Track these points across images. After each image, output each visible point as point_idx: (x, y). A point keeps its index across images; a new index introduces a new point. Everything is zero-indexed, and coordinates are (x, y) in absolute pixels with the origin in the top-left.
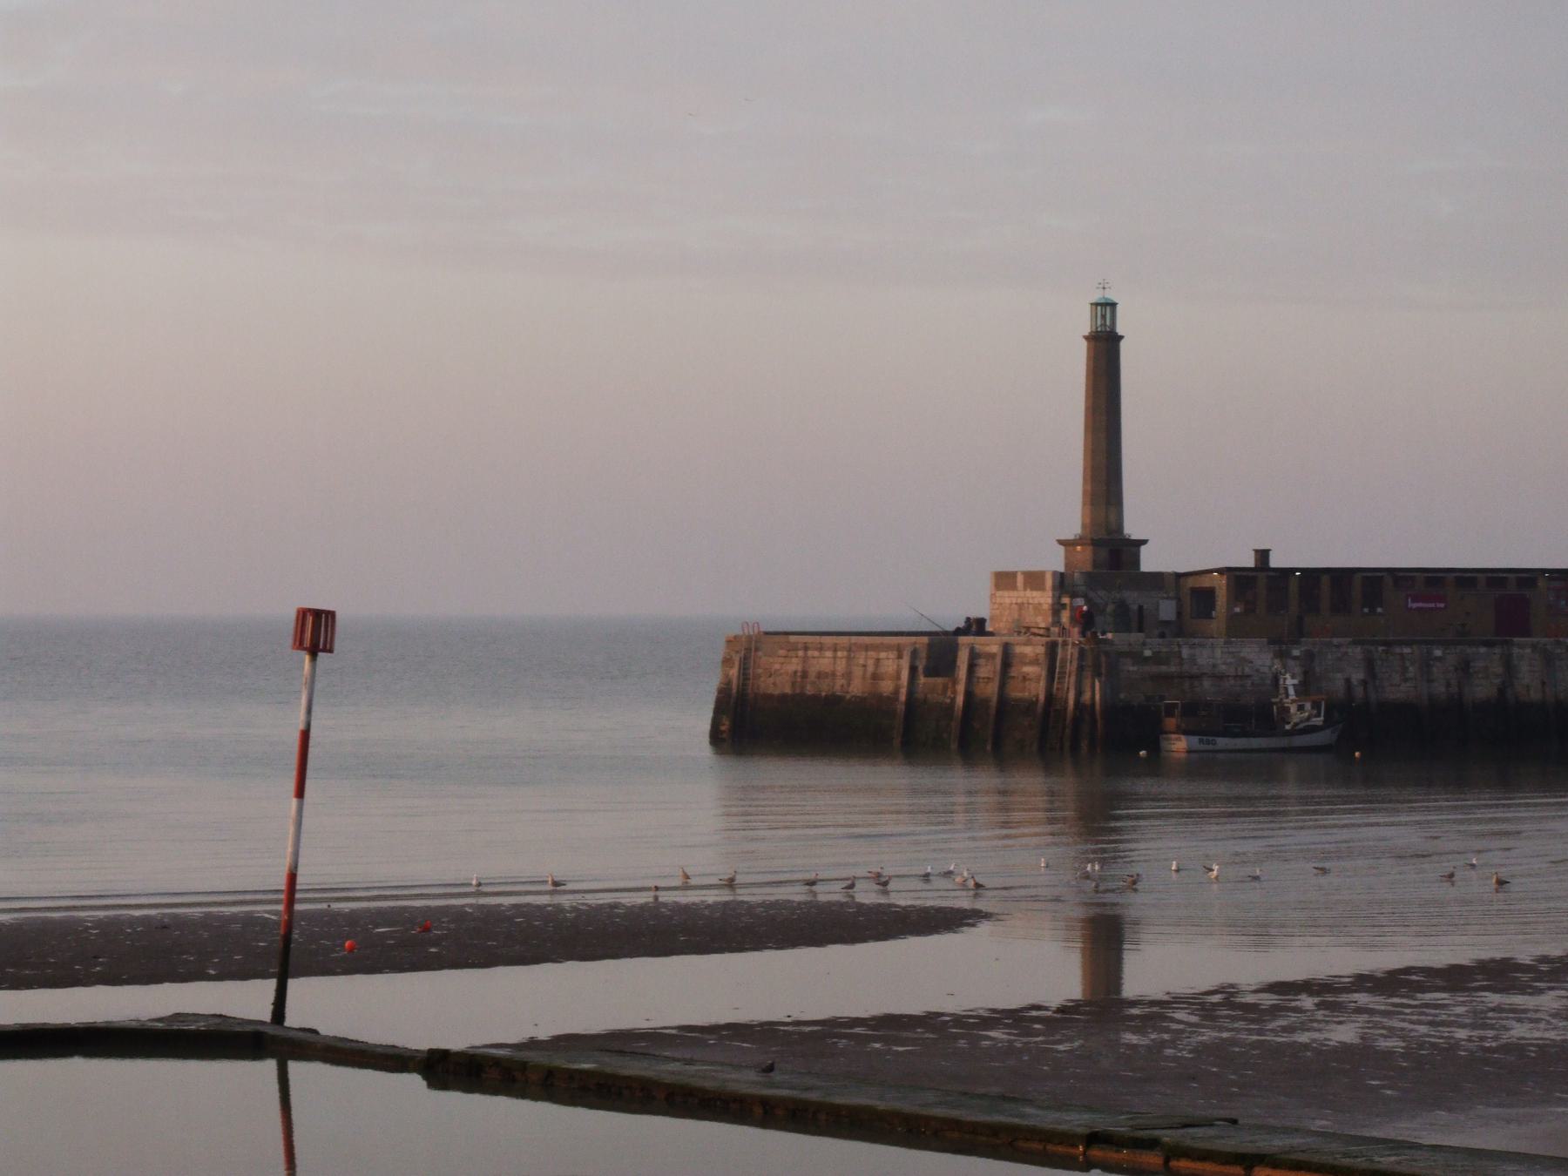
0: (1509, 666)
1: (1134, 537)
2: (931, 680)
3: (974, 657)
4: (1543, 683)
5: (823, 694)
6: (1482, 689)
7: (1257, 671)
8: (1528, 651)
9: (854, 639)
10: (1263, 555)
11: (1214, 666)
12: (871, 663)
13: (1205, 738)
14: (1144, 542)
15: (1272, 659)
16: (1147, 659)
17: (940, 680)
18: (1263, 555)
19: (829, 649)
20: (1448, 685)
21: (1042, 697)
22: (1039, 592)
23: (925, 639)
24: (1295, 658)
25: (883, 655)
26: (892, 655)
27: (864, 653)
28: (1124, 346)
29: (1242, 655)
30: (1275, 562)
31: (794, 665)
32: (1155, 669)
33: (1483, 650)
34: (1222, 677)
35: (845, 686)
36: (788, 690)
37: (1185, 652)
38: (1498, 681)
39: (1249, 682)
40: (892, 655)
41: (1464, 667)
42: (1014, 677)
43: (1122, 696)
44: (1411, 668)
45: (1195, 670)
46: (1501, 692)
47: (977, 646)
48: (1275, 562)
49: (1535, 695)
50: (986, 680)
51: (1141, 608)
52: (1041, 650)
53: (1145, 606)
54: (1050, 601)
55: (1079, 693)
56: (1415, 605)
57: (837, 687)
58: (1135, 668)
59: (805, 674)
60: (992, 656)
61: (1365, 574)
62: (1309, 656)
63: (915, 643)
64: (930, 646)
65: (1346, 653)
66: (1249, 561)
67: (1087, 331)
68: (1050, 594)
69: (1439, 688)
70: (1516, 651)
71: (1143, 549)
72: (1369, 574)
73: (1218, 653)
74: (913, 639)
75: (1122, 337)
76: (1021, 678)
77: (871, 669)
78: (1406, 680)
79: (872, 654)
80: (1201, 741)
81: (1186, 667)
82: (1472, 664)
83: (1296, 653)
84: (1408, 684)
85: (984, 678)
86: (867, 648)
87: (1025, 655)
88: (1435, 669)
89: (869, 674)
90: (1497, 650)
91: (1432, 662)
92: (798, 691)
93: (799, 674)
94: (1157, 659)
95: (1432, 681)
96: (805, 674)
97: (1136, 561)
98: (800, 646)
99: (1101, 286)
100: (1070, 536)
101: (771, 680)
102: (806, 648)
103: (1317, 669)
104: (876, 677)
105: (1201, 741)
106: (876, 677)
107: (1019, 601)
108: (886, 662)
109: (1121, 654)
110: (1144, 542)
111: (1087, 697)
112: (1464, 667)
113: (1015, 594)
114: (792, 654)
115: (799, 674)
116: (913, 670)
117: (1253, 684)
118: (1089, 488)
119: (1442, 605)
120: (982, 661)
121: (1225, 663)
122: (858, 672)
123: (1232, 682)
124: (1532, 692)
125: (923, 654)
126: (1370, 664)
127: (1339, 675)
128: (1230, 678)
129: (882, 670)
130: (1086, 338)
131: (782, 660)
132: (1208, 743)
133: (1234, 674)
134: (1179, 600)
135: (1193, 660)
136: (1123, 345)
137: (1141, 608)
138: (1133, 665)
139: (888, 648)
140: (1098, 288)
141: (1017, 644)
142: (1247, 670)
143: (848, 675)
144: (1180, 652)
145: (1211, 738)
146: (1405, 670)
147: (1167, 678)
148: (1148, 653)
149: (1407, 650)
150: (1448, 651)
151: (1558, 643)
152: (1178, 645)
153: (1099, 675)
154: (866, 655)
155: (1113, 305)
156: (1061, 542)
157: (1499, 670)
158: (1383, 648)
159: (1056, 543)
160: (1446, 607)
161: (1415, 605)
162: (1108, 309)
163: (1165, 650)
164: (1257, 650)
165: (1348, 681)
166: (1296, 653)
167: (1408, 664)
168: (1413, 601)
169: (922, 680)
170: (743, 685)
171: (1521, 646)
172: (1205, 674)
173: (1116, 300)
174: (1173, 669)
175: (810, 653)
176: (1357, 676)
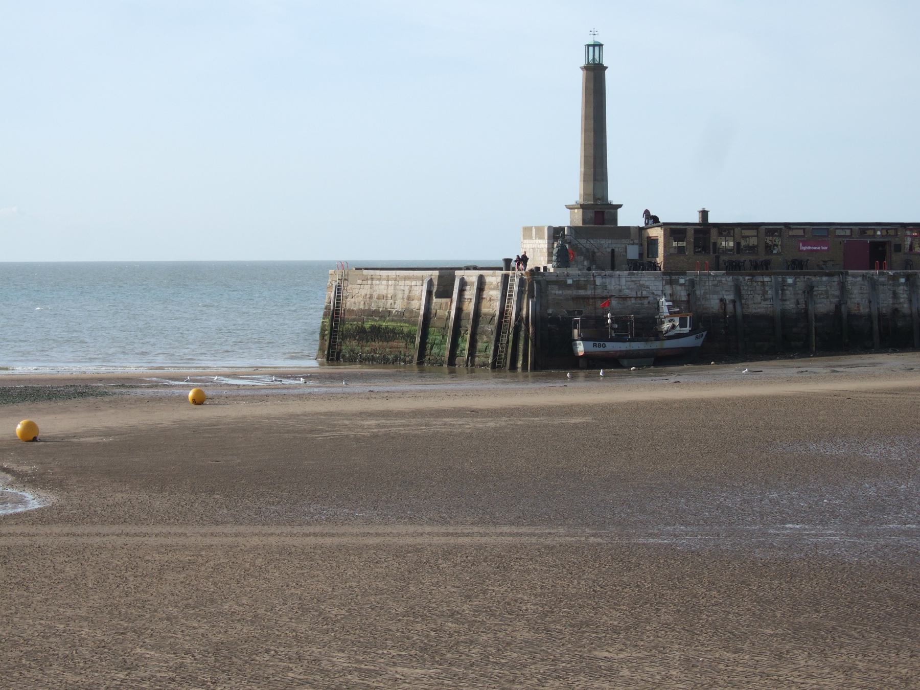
0: (842, 287)
1: (614, 203)
2: (439, 300)
3: (463, 283)
4: (870, 302)
5: (381, 309)
6: (824, 305)
7: (653, 293)
8: (860, 279)
9: (398, 272)
10: (704, 214)
11: (620, 291)
12: (407, 289)
13: (597, 343)
14: (620, 206)
15: (663, 286)
16: (570, 285)
17: (444, 300)
18: (704, 214)
19: (384, 279)
20: (798, 303)
21: (497, 313)
22: (542, 240)
23: (437, 273)
24: (682, 285)
25: (414, 283)
26: (419, 283)
27: (404, 282)
28: (608, 75)
29: (641, 282)
30: (711, 220)
31: (366, 290)
32: (575, 292)
33: (824, 279)
34: (625, 298)
35: (393, 304)
36: (362, 307)
37: (598, 281)
38: (835, 300)
39: (646, 302)
40: (419, 283)
41: (810, 290)
42: (485, 298)
43: (550, 311)
44: (769, 292)
45: (605, 294)
46: (838, 307)
47: (465, 277)
48: (711, 220)
49: (864, 310)
50: (469, 300)
51: (613, 251)
52: (499, 279)
53: (616, 250)
54: (546, 246)
55: (519, 309)
56: (805, 248)
57: (388, 305)
58: (560, 292)
59: (371, 297)
60: (472, 283)
61: (767, 227)
62: (692, 283)
63: (431, 275)
64: (440, 277)
65: (720, 281)
66: (696, 219)
67: (583, 63)
68: (547, 240)
69: (790, 305)
70: (850, 279)
71: (619, 210)
72: (771, 227)
73: (623, 281)
74: (430, 272)
75: (607, 68)
76: (488, 299)
77: (407, 293)
78: (765, 300)
79: (408, 282)
80: (594, 345)
81: (599, 292)
82: (815, 289)
83: (682, 281)
84: (766, 303)
85: (468, 299)
86: (405, 278)
87: (491, 284)
88: (787, 292)
89: (406, 296)
90: (836, 279)
91: (785, 288)
92: (367, 308)
93: (368, 296)
94: (577, 285)
95: (785, 300)
96: (371, 297)
97: (615, 219)
98: (369, 277)
99: (593, 32)
100: (572, 202)
101: (353, 300)
102: (372, 279)
103: (698, 292)
104: (409, 298)
105: (594, 345)
106: (409, 298)
107: (533, 246)
108: (415, 288)
109: (549, 283)
110: (620, 206)
111: (524, 312)
112: (810, 290)
113: (532, 241)
114: (365, 282)
115: (368, 296)
116: (429, 293)
117: (649, 302)
118: (583, 170)
119: (826, 248)
120: (468, 288)
121: (628, 289)
122: (400, 295)
123: (633, 301)
124: (861, 308)
125: (436, 282)
126: (738, 290)
127: (715, 296)
128: (633, 299)
129: (412, 294)
130: (582, 68)
131: (358, 287)
132: (600, 346)
133: (635, 296)
134: (641, 245)
135: (604, 287)
136: (607, 72)
137: (613, 251)
138: (559, 290)
139: (415, 278)
140: (590, 35)
141: (488, 275)
142: (645, 293)
143: (394, 297)
144: (595, 281)
145: (602, 343)
146: (765, 293)
147: (585, 299)
148: (570, 282)
149: (766, 279)
150: (798, 280)
151: (881, 274)
152: (593, 276)
153: (533, 297)
154: (405, 283)
155: (600, 46)
156: (647, 213)
157: (837, 293)
158: (749, 278)
159: (565, 207)
160: (828, 248)
161: (805, 248)
162: (597, 49)
163: (583, 279)
164: (653, 279)
165: (722, 300)
166: (682, 281)
167: (767, 288)
168: (804, 245)
169: (435, 300)
170: (337, 307)
171: (854, 276)
172: (612, 296)
173: (602, 43)
174: (589, 292)
175: (374, 282)
176: (729, 297)
